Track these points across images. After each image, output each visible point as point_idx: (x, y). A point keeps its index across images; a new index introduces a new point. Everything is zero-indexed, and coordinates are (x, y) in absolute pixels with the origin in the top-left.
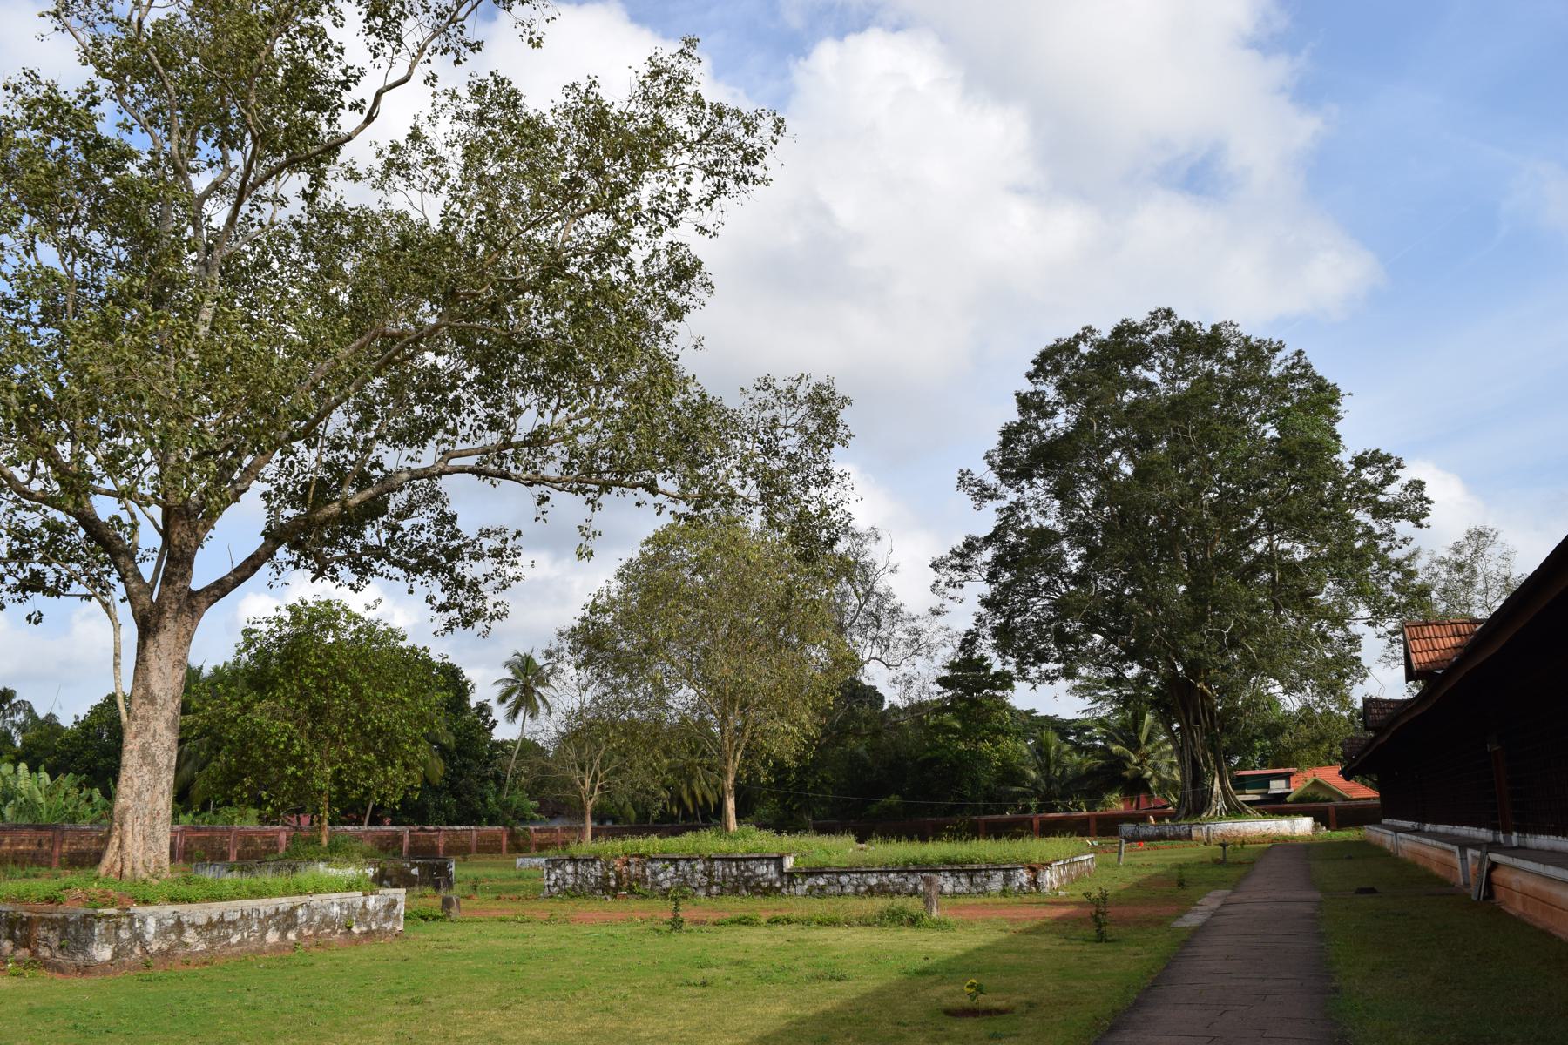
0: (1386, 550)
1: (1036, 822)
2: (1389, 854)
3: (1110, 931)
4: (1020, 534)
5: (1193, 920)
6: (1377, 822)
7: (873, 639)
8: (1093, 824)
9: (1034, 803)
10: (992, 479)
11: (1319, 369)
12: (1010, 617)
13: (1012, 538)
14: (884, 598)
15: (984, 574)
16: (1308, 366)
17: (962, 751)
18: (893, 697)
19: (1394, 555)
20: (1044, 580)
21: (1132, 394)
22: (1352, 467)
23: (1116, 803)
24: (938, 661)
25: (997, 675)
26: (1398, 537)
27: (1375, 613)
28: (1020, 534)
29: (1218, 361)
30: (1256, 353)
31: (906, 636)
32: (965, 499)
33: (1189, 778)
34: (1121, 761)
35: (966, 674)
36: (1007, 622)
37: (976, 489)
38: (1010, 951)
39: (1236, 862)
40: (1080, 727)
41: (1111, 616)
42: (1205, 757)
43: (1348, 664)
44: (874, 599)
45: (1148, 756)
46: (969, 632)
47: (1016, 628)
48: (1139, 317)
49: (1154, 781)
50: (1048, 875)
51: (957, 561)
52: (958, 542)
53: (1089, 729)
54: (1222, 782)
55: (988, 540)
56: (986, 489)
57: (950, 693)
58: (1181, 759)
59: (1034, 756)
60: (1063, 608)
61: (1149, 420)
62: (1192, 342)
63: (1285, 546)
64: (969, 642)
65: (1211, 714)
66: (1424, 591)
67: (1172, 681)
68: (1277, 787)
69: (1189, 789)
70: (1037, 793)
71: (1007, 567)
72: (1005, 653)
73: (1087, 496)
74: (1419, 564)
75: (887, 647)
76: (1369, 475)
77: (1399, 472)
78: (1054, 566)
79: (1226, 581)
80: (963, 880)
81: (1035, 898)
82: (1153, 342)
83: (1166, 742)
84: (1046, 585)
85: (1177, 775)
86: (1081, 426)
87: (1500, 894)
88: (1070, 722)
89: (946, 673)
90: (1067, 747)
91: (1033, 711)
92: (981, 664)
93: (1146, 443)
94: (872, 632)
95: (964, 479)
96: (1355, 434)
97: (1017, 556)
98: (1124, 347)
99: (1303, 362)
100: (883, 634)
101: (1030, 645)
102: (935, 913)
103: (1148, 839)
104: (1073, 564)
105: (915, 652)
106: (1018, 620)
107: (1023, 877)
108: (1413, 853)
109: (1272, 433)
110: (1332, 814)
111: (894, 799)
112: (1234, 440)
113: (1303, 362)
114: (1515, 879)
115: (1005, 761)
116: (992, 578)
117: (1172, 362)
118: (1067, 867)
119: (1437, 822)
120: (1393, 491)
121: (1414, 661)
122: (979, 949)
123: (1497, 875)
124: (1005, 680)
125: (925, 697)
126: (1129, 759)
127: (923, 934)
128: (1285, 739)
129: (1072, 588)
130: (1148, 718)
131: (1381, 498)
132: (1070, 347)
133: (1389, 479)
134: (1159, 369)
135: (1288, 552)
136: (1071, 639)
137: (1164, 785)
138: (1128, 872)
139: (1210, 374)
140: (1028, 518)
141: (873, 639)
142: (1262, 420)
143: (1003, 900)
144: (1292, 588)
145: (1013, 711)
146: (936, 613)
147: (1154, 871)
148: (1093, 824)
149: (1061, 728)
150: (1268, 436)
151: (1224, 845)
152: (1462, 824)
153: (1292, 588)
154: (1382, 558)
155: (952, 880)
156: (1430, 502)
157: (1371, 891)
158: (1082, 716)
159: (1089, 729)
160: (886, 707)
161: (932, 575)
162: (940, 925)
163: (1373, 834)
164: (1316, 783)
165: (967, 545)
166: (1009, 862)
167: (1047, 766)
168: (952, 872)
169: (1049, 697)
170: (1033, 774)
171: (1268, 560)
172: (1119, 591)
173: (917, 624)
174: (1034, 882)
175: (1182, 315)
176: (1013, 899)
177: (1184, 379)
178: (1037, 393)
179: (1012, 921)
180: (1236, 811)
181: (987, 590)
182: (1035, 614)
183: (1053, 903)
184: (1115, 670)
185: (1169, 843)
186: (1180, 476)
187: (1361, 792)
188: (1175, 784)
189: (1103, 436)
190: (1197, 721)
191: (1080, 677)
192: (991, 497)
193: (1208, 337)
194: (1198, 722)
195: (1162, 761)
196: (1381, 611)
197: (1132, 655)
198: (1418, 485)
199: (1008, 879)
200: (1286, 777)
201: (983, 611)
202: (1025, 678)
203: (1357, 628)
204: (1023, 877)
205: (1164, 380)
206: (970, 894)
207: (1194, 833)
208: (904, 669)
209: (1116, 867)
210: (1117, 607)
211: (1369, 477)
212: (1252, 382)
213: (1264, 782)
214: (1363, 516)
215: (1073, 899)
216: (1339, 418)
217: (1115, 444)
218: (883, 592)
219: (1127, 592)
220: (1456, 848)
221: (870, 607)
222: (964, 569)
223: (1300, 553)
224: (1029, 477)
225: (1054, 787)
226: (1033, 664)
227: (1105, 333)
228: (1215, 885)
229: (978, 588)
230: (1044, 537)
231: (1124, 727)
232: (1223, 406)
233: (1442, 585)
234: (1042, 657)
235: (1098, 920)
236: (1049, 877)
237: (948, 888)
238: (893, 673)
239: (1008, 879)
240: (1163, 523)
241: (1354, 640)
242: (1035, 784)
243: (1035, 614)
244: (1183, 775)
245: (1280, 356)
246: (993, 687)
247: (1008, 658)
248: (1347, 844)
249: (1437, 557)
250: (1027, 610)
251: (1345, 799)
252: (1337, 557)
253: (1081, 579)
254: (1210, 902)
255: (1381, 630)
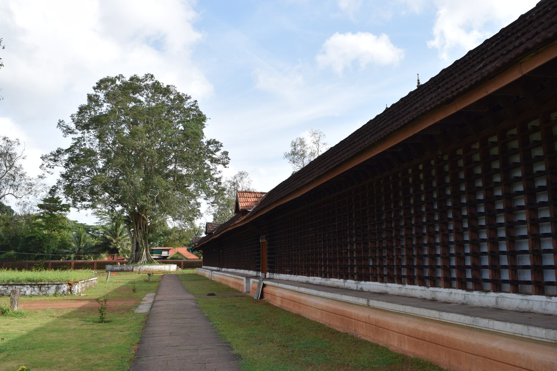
0: (213, 174)
1: (73, 264)
2: (208, 279)
3: (108, 316)
4: (81, 150)
5: (144, 309)
6: (201, 267)
7: (11, 186)
8: (95, 265)
9: (73, 256)
10: (73, 126)
11: (201, 109)
12: (72, 182)
13: (77, 151)
14: (18, 169)
15: (64, 164)
16: (197, 107)
17: (45, 234)
18: (17, 210)
19: (216, 176)
20: (88, 169)
21: (134, 104)
22: (206, 144)
23: (105, 257)
24: (39, 197)
25: (63, 205)
26: (218, 170)
27: (207, 195)
28: (81, 150)
29: (167, 98)
30: (181, 98)
31: (26, 186)
32: (60, 132)
33: (135, 249)
34: (109, 242)
35: (51, 204)
36: (71, 184)
37: (65, 129)
38: (53, 331)
39: (154, 282)
40: (95, 229)
41: (113, 187)
42: (141, 241)
43: (195, 212)
44: (14, 169)
45: (119, 240)
46: (54, 186)
47: (74, 187)
48: (141, 76)
49: (121, 249)
50: (77, 286)
51: (52, 157)
52: (54, 150)
53: (97, 229)
54: (146, 251)
55: (67, 151)
56: (69, 129)
57: (43, 211)
58: (133, 242)
59: (75, 238)
60: (94, 181)
61: (137, 115)
62: (158, 89)
63: (180, 169)
64: (53, 191)
65: (146, 226)
66: (224, 189)
67: (133, 213)
68: (164, 254)
69: (134, 253)
70: (74, 252)
71: (73, 162)
72: (68, 196)
73: (110, 140)
74: (222, 181)
75: (17, 189)
76: (212, 148)
77: (221, 148)
78: (92, 164)
79: (157, 179)
80: (36, 289)
81: (69, 297)
82: (144, 86)
83: (127, 236)
84: (89, 172)
85: (130, 248)
86: (112, 112)
87: (267, 297)
88: (90, 226)
89: (42, 203)
90: (88, 236)
91: (77, 221)
92: (57, 200)
93: (135, 123)
94: (11, 182)
95: (60, 124)
96: (209, 133)
97: (78, 158)
98: (133, 86)
99: (196, 105)
100: (16, 183)
101: (79, 194)
102: (16, 309)
103: (117, 271)
104: (101, 164)
105: (29, 193)
106: (75, 184)
107: (65, 287)
108: (220, 279)
109: (181, 128)
110: (182, 264)
111: (12, 252)
112: (169, 127)
113: (196, 105)
114: (278, 292)
115: (63, 240)
116: (67, 165)
117: (150, 95)
118: (87, 284)
119: (228, 268)
120: (218, 155)
121: (240, 205)
122: (36, 330)
123: (265, 289)
124: (67, 207)
125: (31, 212)
126: (112, 241)
127: (7, 320)
128: (171, 237)
129: (99, 174)
130: (122, 226)
131: (214, 156)
132: (113, 81)
133: (218, 150)
134: (145, 96)
135: (181, 171)
136: (96, 193)
137: (124, 251)
138: (111, 285)
139: (164, 102)
140: (85, 144)
141: (11, 186)
142: (178, 123)
143: (55, 298)
144: (180, 182)
145: (68, 221)
146: (41, 177)
147: (121, 284)
148: (95, 265)
149: (87, 229)
150: (180, 128)
151: (149, 275)
152: (240, 268)
153: (180, 182)
154: (210, 176)
155: (30, 289)
156: (229, 159)
157: (214, 295)
158: (95, 225)
159: (97, 229)
160: (14, 215)
161: (41, 162)
162: (18, 314)
163: (200, 271)
164: (178, 253)
165: (58, 151)
166: (59, 281)
167: (80, 242)
168: (31, 285)
169: (83, 216)
170: (74, 245)
171: (174, 172)
172: (117, 177)
173: (32, 181)
174: (70, 290)
175: (157, 78)
176: (59, 298)
177: (154, 102)
178: (96, 96)
179: (57, 310)
180: (150, 262)
181: (64, 170)
182: (83, 182)
183: (78, 300)
184: (112, 207)
185: (125, 273)
186: (147, 137)
187: (192, 257)
188: (128, 252)
189: (119, 118)
190: (140, 228)
191: (98, 208)
192: (71, 133)
193: (165, 89)
194: (141, 226)
195: (125, 242)
196: (209, 194)
197: (119, 201)
198: (226, 153)
199: (58, 289)
200: (168, 250)
201: (61, 179)
202: (75, 207)
203: (199, 200)
204: (65, 287)
205: (146, 101)
206: (39, 295)
207: (134, 269)
208: (24, 199)
209: (105, 283)
210: (116, 183)
211: (211, 148)
212: (178, 108)
213: (160, 252)
214: (208, 162)
215: (88, 298)
216: (204, 127)
217: (124, 122)
218: (18, 166)
219: (120, 178)
220: (244, 279)
221: (11, 172)
222: (55, 161)
223: (184, 172)
224: (88, 129)
225: (81, 250)
226: (80, 202)
227: (127, 79)
228: (148, 290)
229: (60, 169)
230: (90, 153)
231: (112, 229)
232: (166, 115)
233: (228, 189)
234: (83, 200)
235: (101, 311)
236: (77, 288)
237: (28, 293)
238: (18, 200)
239: (58, 289)
240: (137, 155)
241: (198, 204)
242: (74, 249)
243: (83, 182)
244: (133, 248)
245: (189, 101)
246: (61, 210)
247: (69, 198)
248: (190, 275)
249: (228, 179)
250: (79, 180)
251: (187, 259)
252: (198, 174)
253: (103, 170)
254: (148, 299)
255: (208, 201)
